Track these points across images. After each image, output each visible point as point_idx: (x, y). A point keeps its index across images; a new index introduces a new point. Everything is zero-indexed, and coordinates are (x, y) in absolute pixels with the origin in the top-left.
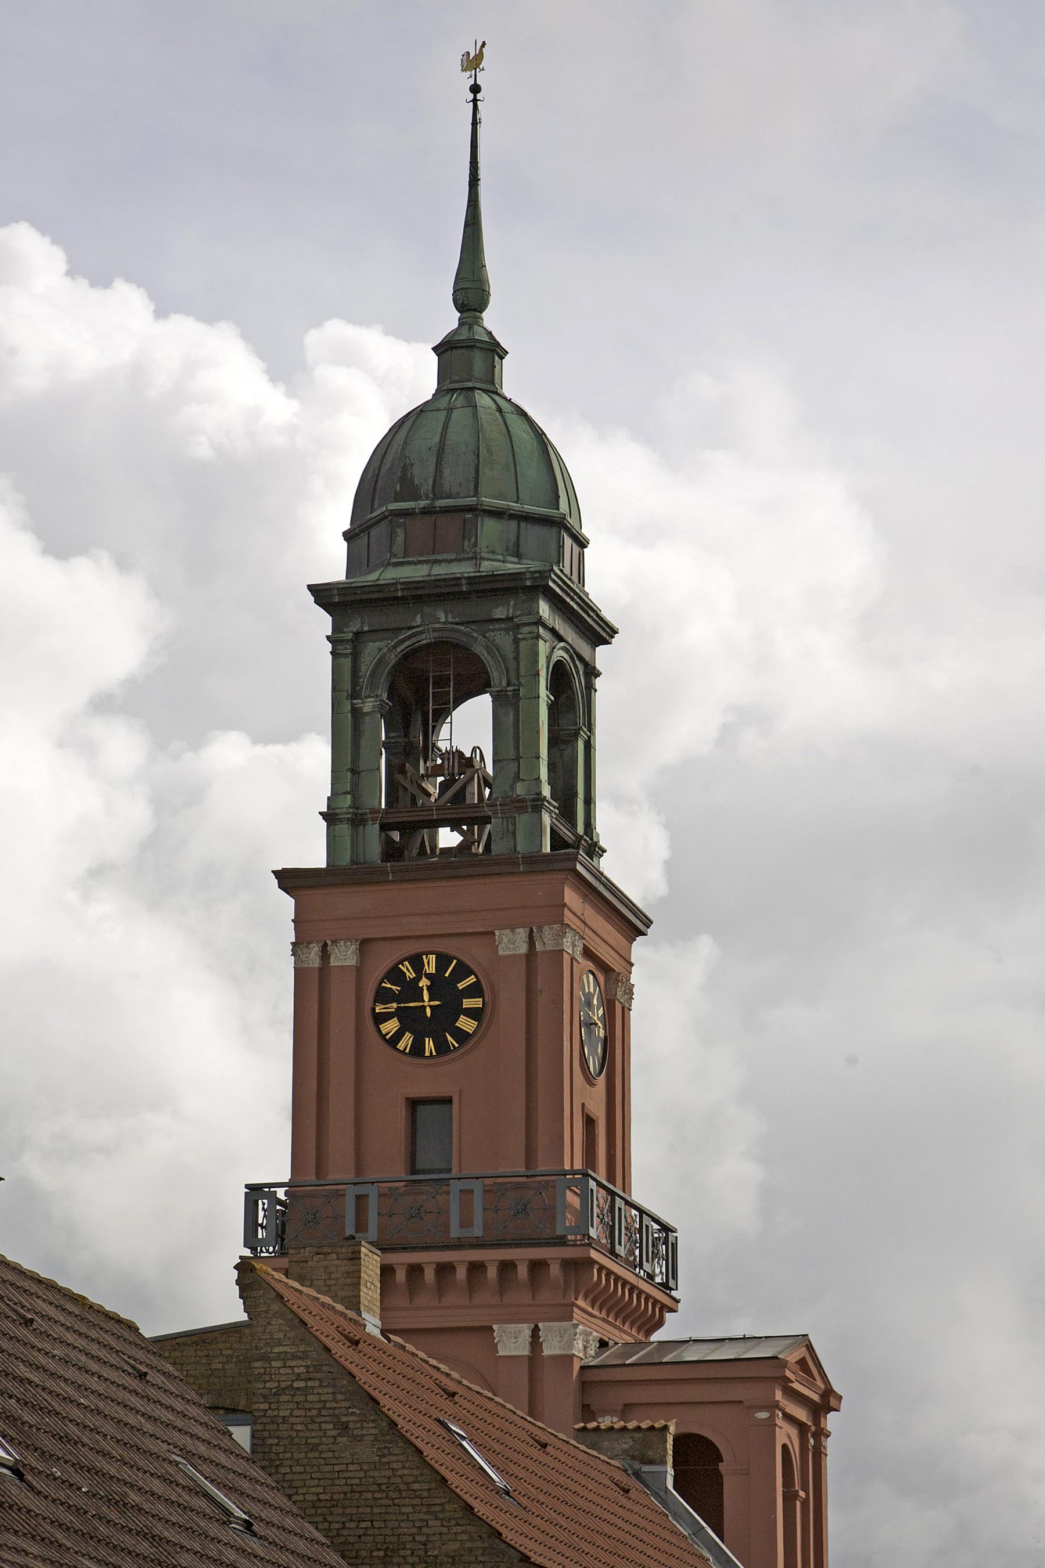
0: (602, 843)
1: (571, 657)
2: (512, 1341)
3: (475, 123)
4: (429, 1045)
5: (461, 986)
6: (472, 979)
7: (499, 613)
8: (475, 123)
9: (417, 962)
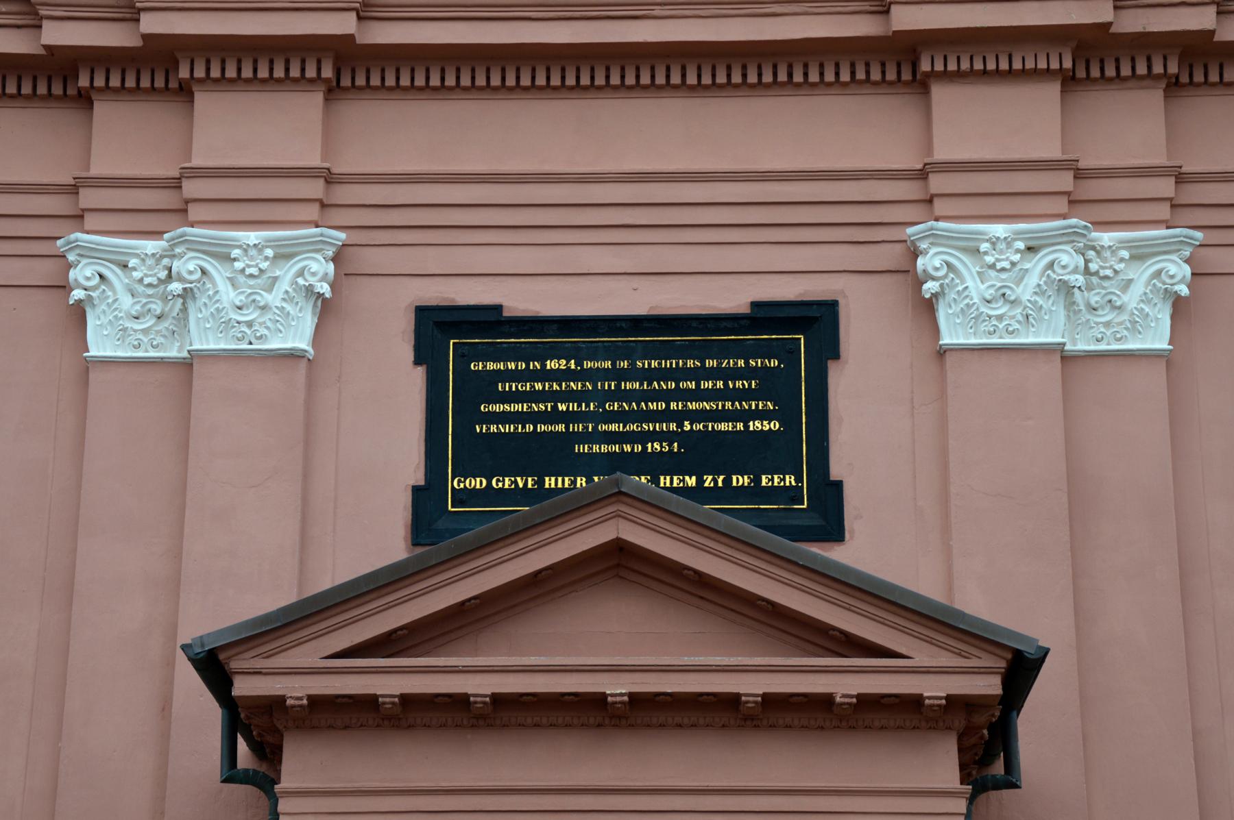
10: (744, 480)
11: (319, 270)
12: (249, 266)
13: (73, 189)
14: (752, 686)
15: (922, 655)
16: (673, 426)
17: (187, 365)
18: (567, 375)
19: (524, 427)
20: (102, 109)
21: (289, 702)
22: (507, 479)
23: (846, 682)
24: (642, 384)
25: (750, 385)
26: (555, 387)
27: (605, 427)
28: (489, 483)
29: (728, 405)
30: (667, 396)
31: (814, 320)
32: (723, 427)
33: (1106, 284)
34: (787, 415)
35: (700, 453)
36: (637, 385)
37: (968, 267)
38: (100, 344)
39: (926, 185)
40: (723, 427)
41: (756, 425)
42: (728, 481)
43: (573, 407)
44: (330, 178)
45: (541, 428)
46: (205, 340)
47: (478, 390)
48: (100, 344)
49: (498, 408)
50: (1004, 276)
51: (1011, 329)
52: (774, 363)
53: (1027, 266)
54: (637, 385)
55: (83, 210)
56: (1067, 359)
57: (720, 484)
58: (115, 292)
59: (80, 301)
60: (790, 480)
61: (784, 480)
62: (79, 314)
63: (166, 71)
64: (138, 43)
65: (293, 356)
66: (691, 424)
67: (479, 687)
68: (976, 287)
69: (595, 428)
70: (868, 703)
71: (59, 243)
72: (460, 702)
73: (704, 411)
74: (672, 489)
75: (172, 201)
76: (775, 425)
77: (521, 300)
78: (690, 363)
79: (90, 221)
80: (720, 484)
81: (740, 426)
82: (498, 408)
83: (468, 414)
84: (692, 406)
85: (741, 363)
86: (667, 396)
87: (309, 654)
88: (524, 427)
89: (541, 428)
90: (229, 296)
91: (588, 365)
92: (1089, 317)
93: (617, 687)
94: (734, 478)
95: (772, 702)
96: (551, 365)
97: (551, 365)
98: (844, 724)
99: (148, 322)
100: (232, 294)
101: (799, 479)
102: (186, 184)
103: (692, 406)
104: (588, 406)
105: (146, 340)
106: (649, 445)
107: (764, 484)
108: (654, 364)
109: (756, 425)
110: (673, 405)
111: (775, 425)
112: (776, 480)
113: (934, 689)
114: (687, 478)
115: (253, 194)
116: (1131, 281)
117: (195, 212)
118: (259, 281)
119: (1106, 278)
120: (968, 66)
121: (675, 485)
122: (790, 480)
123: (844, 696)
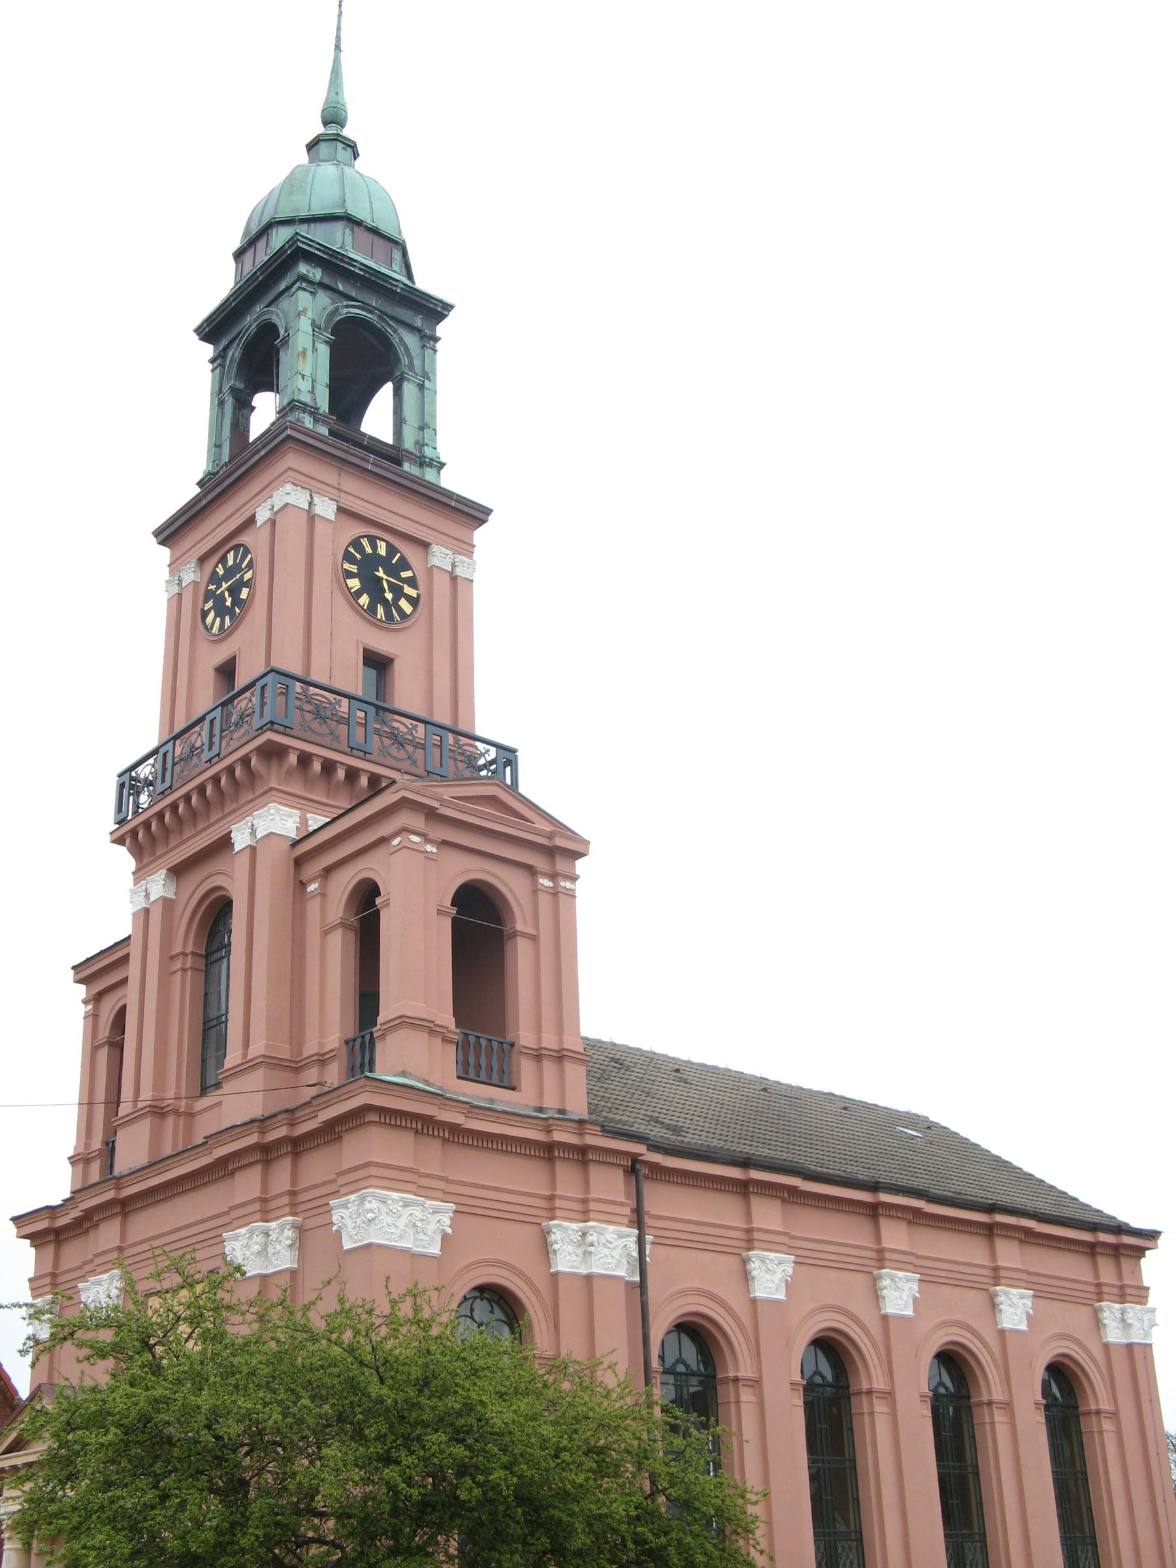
0: (442, 460)
1: (379, 317)
2: (241, 839)
3: (340, 14)
4: (227, 619)
5: (358, 556)
6: (249, 557)
7: (283, 286)
8: (340, 14)
9: (223, 560)
38: (347, 1245)
39: (234, 1217)
48: (347, 1245)
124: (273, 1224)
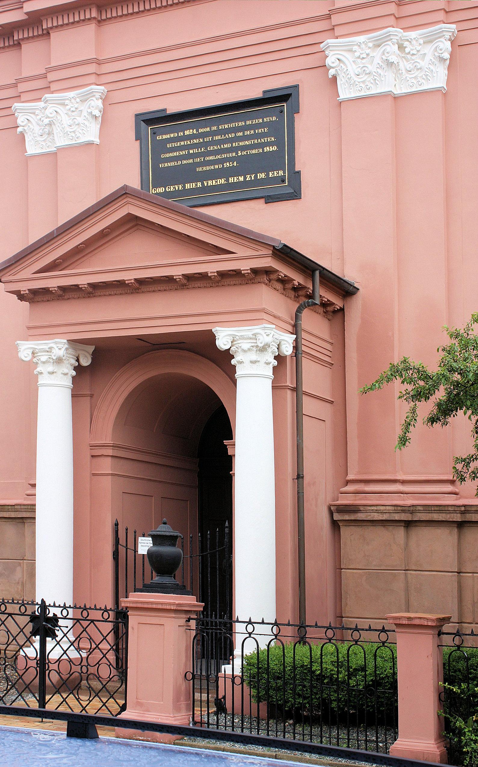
10: (263, 175)
11: (96, 104)
12: (72, 107)
13: (328, 17)
14: (177, 272)
15: (241, 250)
16: (234, 154)
17: (54, 155)
18: (193, 137)
19: (177, 163)
20: (26, 47)
21: (22, 292)
22: (275, 172)
23: (213, 266)
24: (221, 136)
25: (264, 130)
26: (189, 143)
27: (208, 158)
28: (165, 189)
29: (256, 141)
30: (231, 140)
31: (289, 95)
32: (254, 152)
33: (413, 57)
34: (279, 143)
35: (246, 165)
36: (220, 137)
37: (348, 57)
40: (254, 152)
41: (267, 149)
42: (256, 177)
43: (196, 151)
44: (99, 62)
45: (184, 162)
46: (61, 141)
47: (160, 148)
49: (168, 155)
50: (364, 61)
51: (368, 87)
52: (274, 118)
53: (374, 54)
54: (220, 137)
55: (334, 26)
56: (396, 98)
57: (253, 179)
58: (347, 67)
59: (21, 132)
60: (281, 173)
61: (278, 173)
62: (22, 137)
63: (37, 25)
64: (25, 17)
65: (89, 144)
66: (241, 152)
67: (83, 281)
68: (352, 69)
69: (204, 159)
70: (223, 275)
71: (322, 45)
72: (76, 288)
73: (246, 145)
74: (157, 194)
75: (44, 84)
76: (275, 148)
77: (174, 106)
78: (240, 124)
79: (24, 97)
80: (253, 179)
81: (261, 150)
82: (168, 155)
83: (157, 160)
84: (241, 144)
85: (261, 121)
86: (231, 140)
87: (27, 273)
88: (177, 163)
89: (184, 162)
90: (66, 120)
91: (201, 131)
92: (407, 75)
93: (129, 277)
94: (258, 175)
95: (189, 278)
96: (187, 133)
97: (187, 133)
98: (220, 284)
99: (45, 136)
100: (355, 67)
101: (284, 173)
102: (49, 75)
103: (241, 144)
104: (201, 149)
105: (415, 82)
106: (225, 164)
107: (270, 176)
108: (226, 126)
109: (267, 149)
110: (234, 145)
111: (275, 148)
112: (275, 174)
113: (245, 266)
114: (240, 177)
115: (71, 76)
116: (425, 54)
117: (54, 87)
118: (76, 113)
119: (413, 55)
120: (149, 6)
121: (214, 184)
122: (281, 173)
123: (211, 273)
124: (413, 34)
